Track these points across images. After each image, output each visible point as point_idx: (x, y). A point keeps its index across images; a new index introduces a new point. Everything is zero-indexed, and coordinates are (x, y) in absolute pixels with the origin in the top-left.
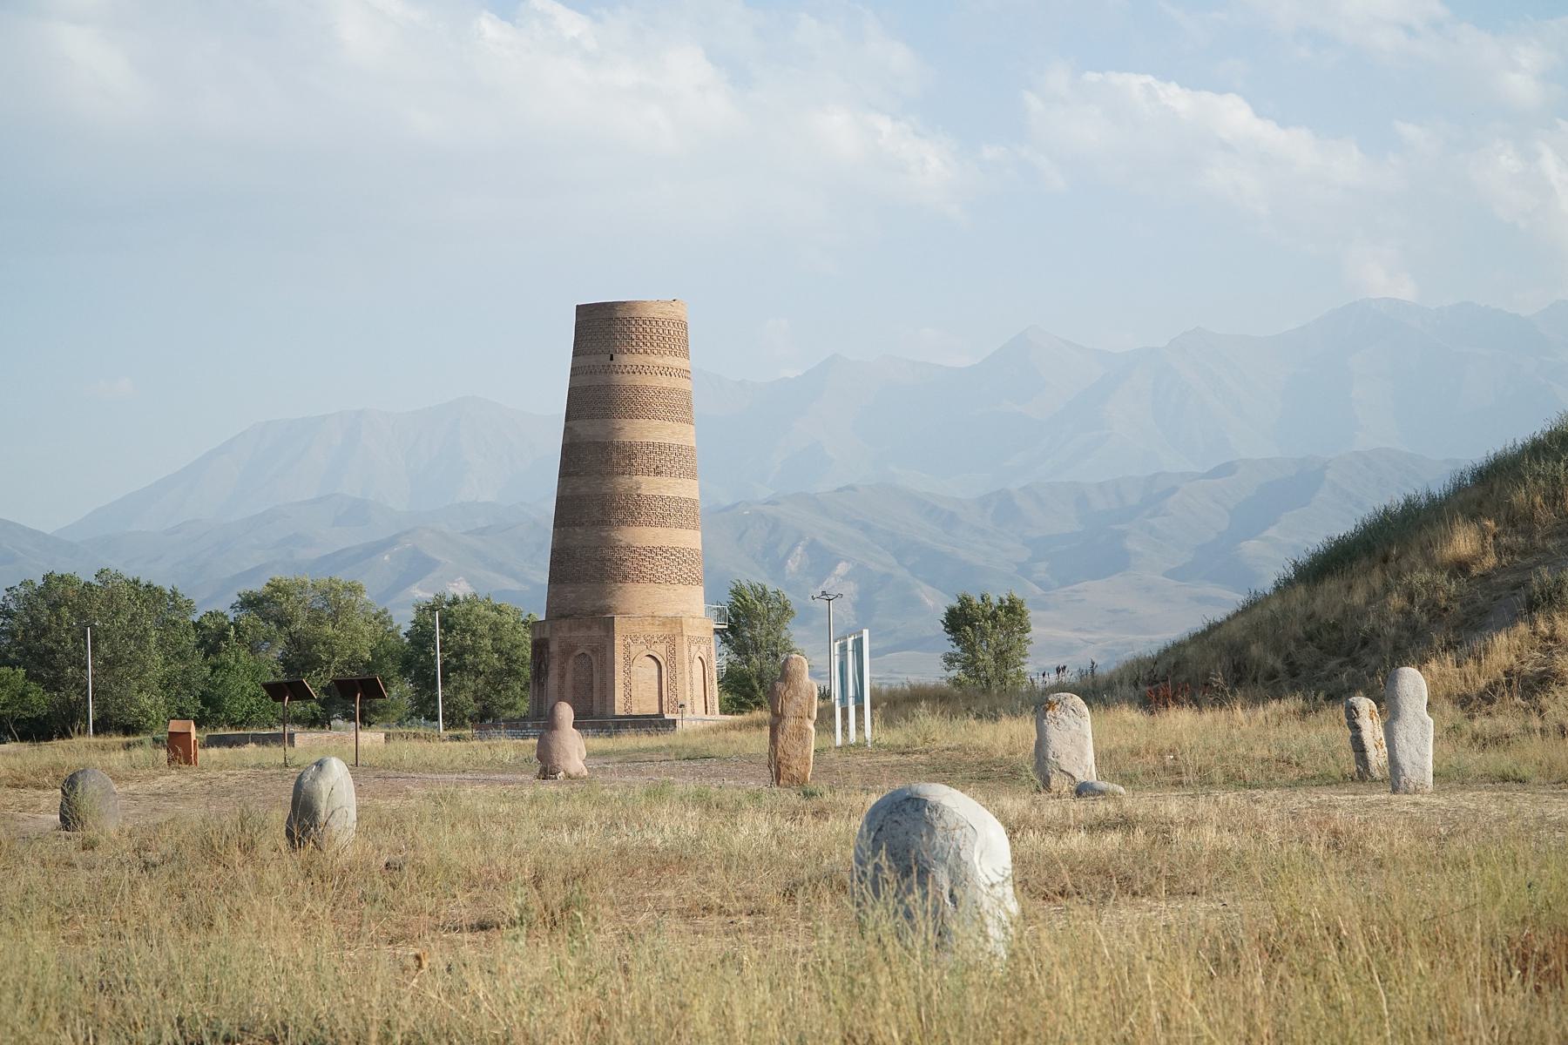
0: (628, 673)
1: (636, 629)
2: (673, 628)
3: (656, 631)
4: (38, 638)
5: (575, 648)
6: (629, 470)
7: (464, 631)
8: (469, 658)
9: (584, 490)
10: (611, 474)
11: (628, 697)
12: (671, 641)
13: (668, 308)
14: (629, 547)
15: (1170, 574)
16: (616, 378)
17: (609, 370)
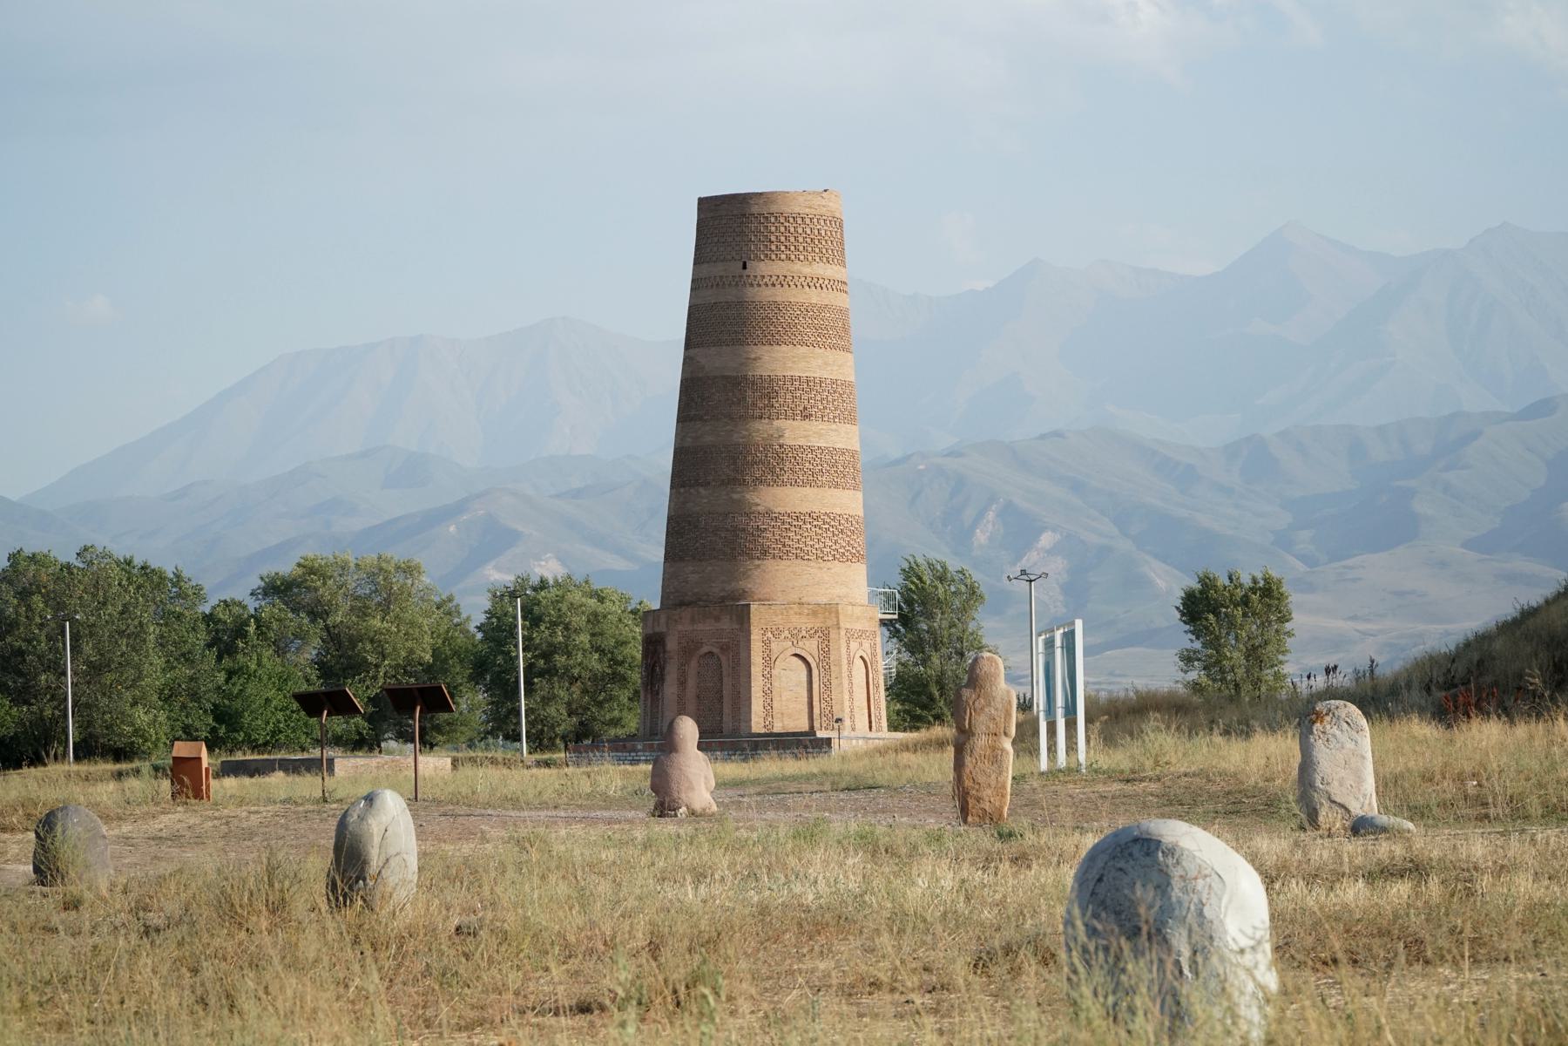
0: (768, 677)
1: (778, 619)
3: (804, 623)
5: (699, 644)
6: (768, 414)
7: (554, 624)
9: (709, 439)
10: (745, 418)
11: (769, 707)
13: (817, 201)
14: (768, 513)
16: (753, 293)
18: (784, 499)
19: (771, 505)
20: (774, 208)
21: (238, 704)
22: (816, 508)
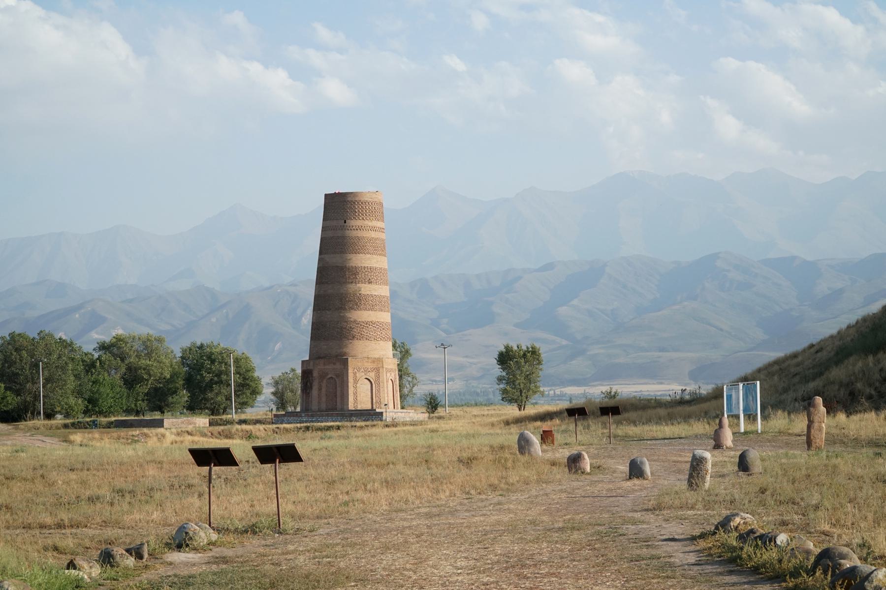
0: (355, 388)
1: (359, 364)
2: (378, 362)
3: (369, 365)
4: (9, 367)
5: (327, 374)
6: (355, 281)
7: (220, 363)
8: (224, 377)
10: (345, 283)
11: (356, 400)
12: (377, 370)
13: (374, 196)
14: (355, 321)
15: (517, 325)
17: (343, 228)
18: (362, 315)
19: (355, 318)
20: (357, 199)
21: (97, 396)
22: (374, 319)
